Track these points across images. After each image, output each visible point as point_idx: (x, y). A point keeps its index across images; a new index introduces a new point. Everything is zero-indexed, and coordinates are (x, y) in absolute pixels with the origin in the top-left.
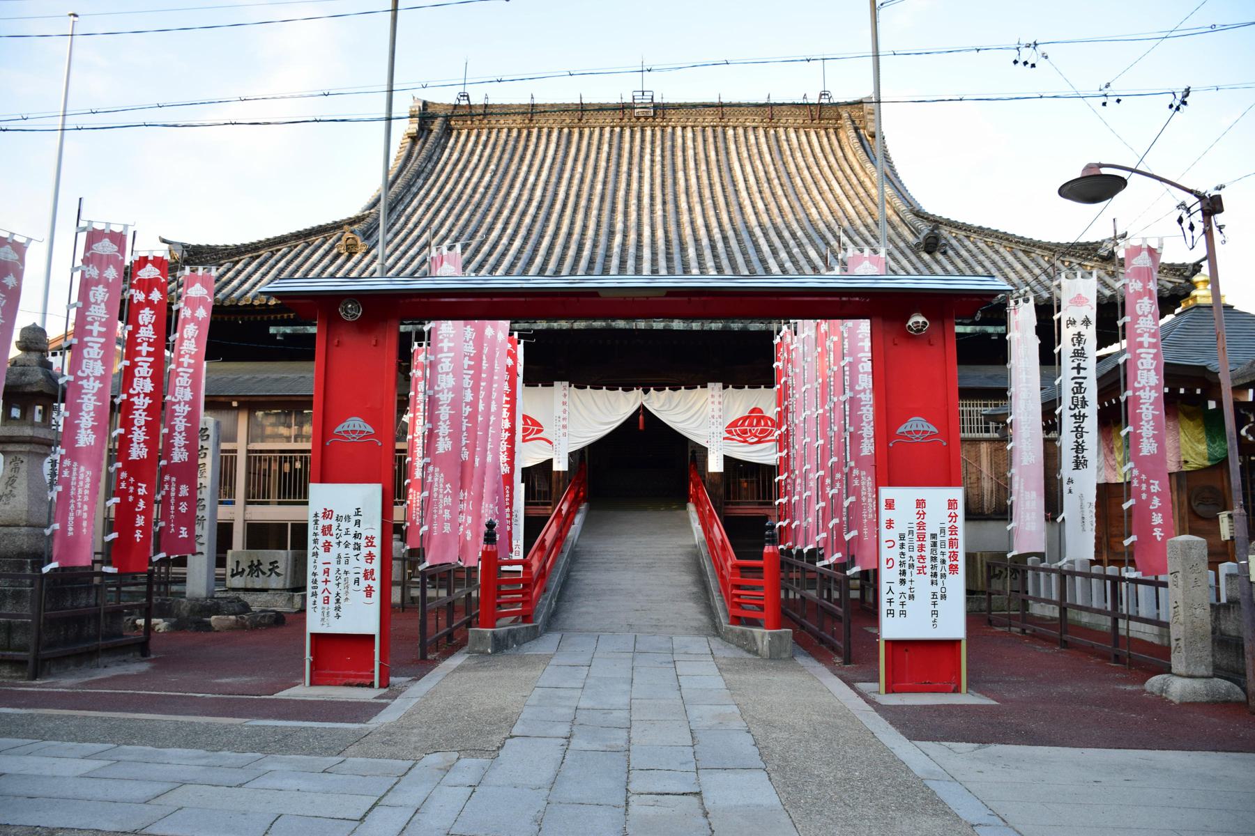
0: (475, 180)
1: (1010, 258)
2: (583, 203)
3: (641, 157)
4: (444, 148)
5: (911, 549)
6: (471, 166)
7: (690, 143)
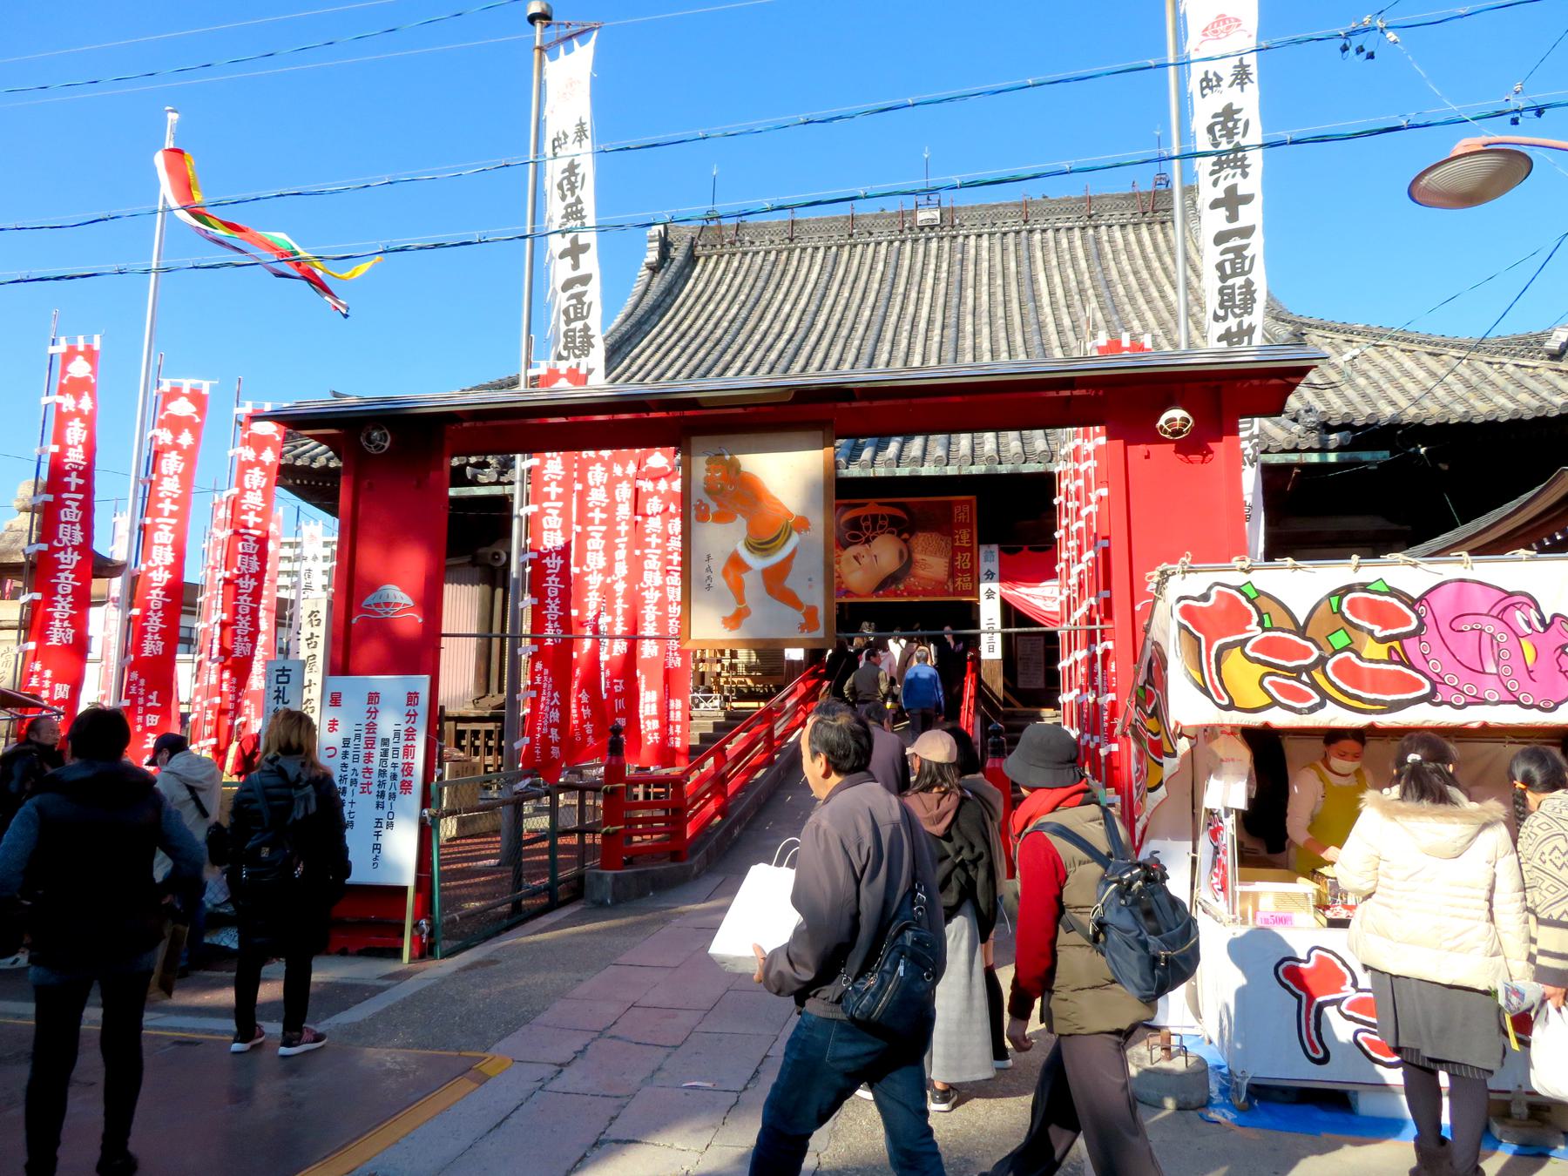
0: (719, 313)
1: (1409, 364)
2: (844, 332)
3: (923, 276)
4: (689, 277)
5: (356, 759)
6: (717, 297)
7: (985, 254)
